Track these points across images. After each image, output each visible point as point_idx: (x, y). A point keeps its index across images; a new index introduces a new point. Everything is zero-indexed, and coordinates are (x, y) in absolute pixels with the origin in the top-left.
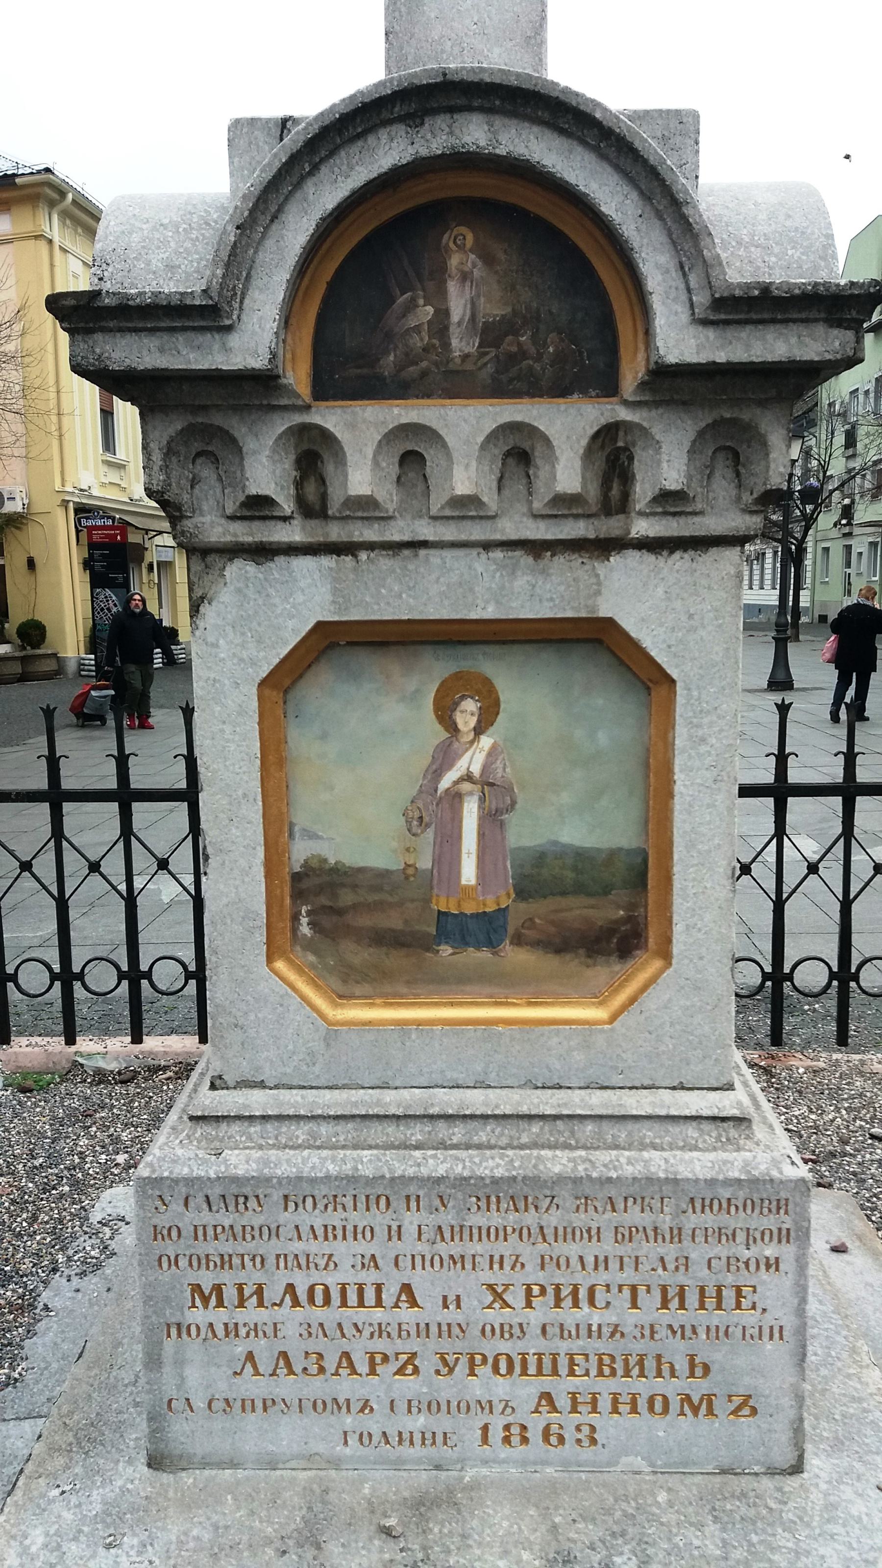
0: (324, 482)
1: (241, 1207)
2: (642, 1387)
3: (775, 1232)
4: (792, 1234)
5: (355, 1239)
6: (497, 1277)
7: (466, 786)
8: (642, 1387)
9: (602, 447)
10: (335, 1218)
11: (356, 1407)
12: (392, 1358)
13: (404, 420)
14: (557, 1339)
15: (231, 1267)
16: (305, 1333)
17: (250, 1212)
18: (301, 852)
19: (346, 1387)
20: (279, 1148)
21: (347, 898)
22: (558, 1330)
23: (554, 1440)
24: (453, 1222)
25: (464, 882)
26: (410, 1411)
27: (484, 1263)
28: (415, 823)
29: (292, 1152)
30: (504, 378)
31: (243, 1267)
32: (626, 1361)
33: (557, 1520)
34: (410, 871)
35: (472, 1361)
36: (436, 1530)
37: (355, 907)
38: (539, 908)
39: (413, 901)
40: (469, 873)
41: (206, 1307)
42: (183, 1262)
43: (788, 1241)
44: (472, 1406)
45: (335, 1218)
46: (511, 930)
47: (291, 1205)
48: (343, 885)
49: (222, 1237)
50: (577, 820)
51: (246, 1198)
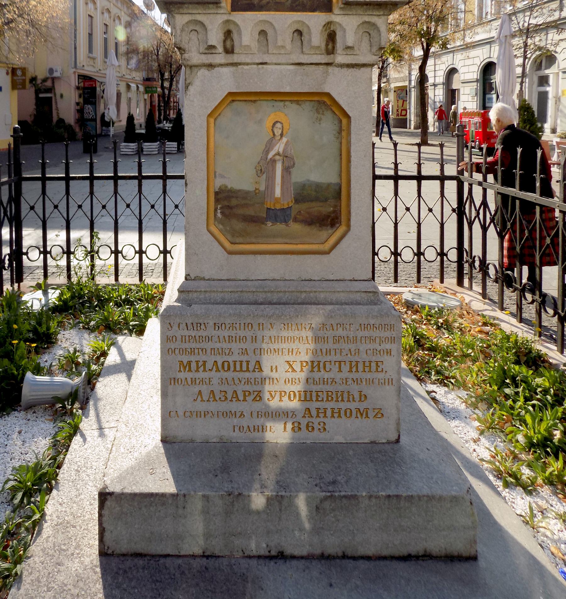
0: (233, 41)
1: (199, 328)
2: (343, 406)
3: (390, 338)
4: (396, 339)
5: (240, 342)
6: (290, 358)
7: (277, 157)
8: (343, 406)
9: (326, 30)
10: (233, 333)
11: (238, 414)
12: (252, 393)
13: (261, 19)
14: (312, 385)
15: (194, 354)
16: (220, 383)
17: (202, 330)
18: (218, 183)
19: (234, 406)
20: (211, 304)
21: (234, 202)
22: (312, 381)
23: (310, 429)
24: (275, 335)
25: (276, 196)
26: (258, 417)
27: (286, 351)
28: (259, 172)
29: (217, 306)
30: (294, 5)
31: (199, 354)
32: (337, 394)
33: (314, 462)
34: (257, 191)
35: (281, 394)
36: (271, 466)
37: (237, 206)
38: (304, 207)
39: (258, 203)
40: (278, 192)
41: (185, 372)
42: (177, 351)
43: (394, 343)
44: (281, 414)
45: (233, 333)
46: (293, 216)
47: (217, 327)
48: (233, 197)
49: (191, 341)
50: (317, 171)
51: (201, 324)
